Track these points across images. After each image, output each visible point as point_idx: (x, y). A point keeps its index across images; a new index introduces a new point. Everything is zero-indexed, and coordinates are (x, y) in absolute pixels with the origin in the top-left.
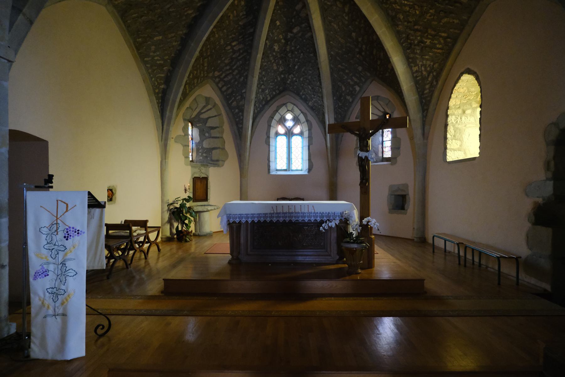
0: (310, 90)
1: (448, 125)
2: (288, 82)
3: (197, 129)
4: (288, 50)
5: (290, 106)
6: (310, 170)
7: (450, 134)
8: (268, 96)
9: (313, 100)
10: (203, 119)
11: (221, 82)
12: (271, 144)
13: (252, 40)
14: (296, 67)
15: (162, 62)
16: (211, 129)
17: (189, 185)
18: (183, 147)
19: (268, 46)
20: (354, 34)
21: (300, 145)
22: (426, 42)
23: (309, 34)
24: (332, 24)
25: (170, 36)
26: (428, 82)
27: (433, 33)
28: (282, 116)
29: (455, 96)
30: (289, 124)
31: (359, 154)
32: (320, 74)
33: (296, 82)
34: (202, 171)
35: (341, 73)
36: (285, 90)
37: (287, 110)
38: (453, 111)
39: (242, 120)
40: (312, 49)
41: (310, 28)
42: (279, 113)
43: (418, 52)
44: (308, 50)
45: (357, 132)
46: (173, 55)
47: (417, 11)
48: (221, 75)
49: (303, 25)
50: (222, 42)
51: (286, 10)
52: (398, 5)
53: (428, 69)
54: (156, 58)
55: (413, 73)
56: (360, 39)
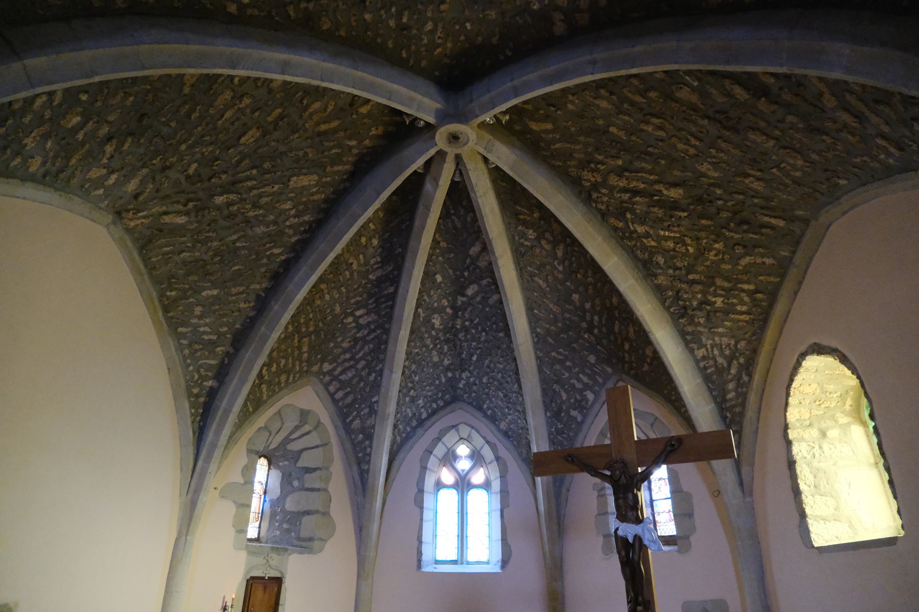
0: (501, 400)
1: (795, 462)
2: (461, 386)
3: (279, 471)
4: (458, 327)
5: (465, 430)
6: (505, 562)
7: (805, 483)
8: (423, 410)
9: (507, 418)
10: (293, 451)
11: (334, 383)
12: (425, 505)
13: (392, 307)
14: (475, 358)
15: (214, 337)
16: (306, 472)
17: (234, 596)
18: (237, 507)
19: (421, 319)
20: (576, 297)
21: (485, 508)
22: (715, 302)
23: (496, 297)
24: (536, 279)
25: (234, 290)
26: (730, 377)
27: (726, 284)
28: (449, 450)
29: (797, 401)
30: (464, 465)
31: (617, 529)
32: (517, 369)
33: (476, 384)
34: (272, 563)
35: (558, 367)
36: (455, 399)
37: (458, 438)
38: (798, 433)
39: (370, 455)
40: (501, 324)
41: (495, 286)
42: (443, 443)
43: (702, 322)
44: (494, 326)
45: (608, 473)
46: (238, 326)
47: (689, 248)
48: (334, 369)
49: (484, 282)
50: (338, 309)
51: (452, 255)
52: (653, 240)
53: (727, 352)
54: (202, 329)
55: (697, 362)
56: (588, 306)
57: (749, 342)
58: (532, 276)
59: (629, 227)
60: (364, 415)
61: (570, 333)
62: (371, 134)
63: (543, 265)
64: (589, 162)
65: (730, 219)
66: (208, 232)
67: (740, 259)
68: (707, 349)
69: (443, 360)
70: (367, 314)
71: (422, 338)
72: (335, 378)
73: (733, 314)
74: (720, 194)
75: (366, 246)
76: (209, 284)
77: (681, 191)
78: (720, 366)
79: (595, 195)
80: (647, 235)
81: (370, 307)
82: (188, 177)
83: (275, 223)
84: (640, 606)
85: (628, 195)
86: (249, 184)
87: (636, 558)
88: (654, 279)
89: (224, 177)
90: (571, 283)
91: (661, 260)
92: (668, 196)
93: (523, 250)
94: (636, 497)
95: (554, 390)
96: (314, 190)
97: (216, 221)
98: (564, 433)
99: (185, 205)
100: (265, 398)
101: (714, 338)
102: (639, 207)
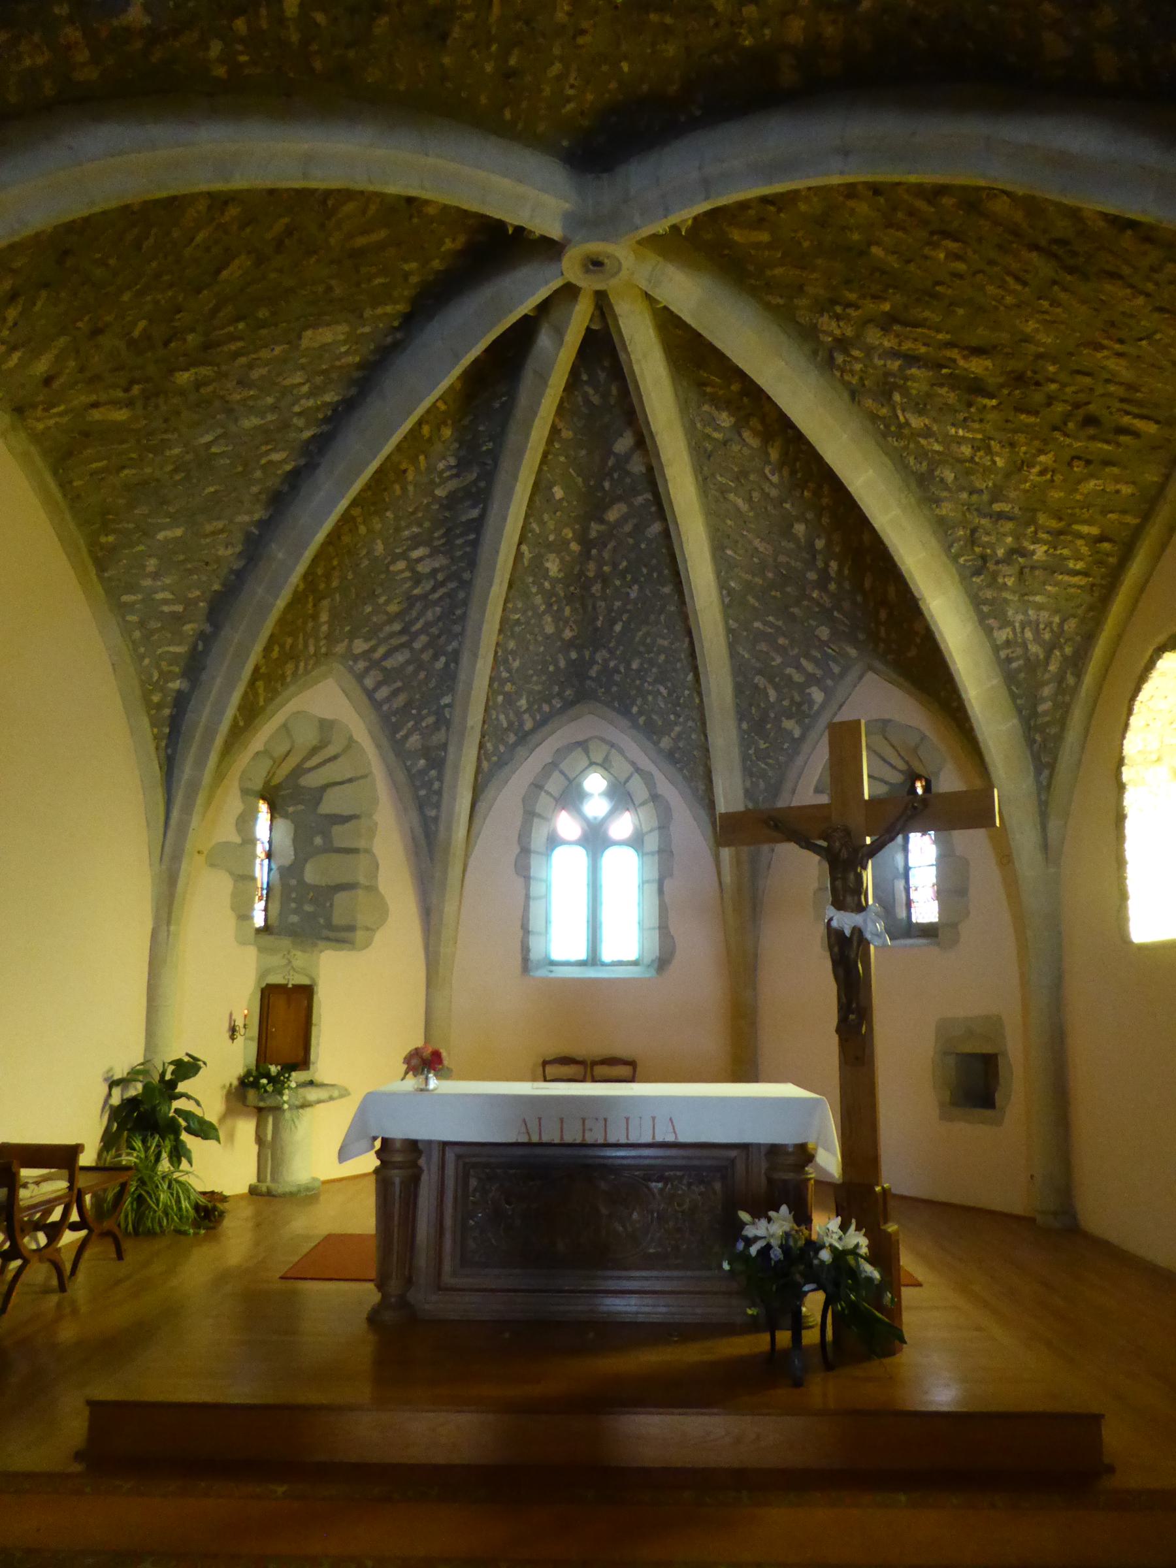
2: (593, 673)
4: (591, 574)
8: (526, 716)
11: (372, 673)
13: (475, 544)
15: (179, 608)
17: (246, 1012)
18: (236, 881)
20: (800, 529)
22: (1033, 553)
24: (731, 496)
26: (1047, 676)
33: (619, 672)
35: (763, 646)
39: (439, 793)
42: (562, 772)
44: (655, 575)
45: (824, 844)
46: (216, 587)
47: (997, 459)
48: (373, 649)
49: (639, 500)
50: (379, 548)
52: (937, 441)
53: (1047, 636)
54: (160, 596)
55: (996, 649)
56: (820, 544)
57: (1083, 621)
58: (723, 491)
59: (897, 417)
60: (427, 727)
61: (789, 589)
62: (443, 249)
63: (744, 474)
64: (834, 302)
65: (1067, 417)
66: (166, 431)
67: (1079, 482)
68: (1014, 630)
69: (563, 631)
70: (430, 556)
71: (526, 595)
72: (375, 664)
73: (1062, 574)
74: (1054, 373)
75: (430, 440)
76: (168, 520)
77: (988, 363)
78: (1032, 658)
79: (840, 359)
80: (927, 433)
81: (436, 543)
82: (132, 343)
83: (274, 408)
84: (853, 1014)
85: (898, 363)
86: (233, 347)
87: (853, 956)
88: (934, 506)
89: (190, 337)
90: (793, 505)
91: (949, 476)
92: (966, 369)
93: (709, 447)
94: (859, 879)
95: (756, 687)
96: (343, 349)
97: (178, 413)
98: (770, 757)
99: (127, 390)
100: (262, 703)
101: (1027, 611)
102: (915, 385)
